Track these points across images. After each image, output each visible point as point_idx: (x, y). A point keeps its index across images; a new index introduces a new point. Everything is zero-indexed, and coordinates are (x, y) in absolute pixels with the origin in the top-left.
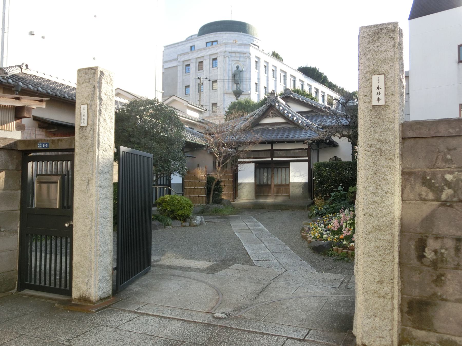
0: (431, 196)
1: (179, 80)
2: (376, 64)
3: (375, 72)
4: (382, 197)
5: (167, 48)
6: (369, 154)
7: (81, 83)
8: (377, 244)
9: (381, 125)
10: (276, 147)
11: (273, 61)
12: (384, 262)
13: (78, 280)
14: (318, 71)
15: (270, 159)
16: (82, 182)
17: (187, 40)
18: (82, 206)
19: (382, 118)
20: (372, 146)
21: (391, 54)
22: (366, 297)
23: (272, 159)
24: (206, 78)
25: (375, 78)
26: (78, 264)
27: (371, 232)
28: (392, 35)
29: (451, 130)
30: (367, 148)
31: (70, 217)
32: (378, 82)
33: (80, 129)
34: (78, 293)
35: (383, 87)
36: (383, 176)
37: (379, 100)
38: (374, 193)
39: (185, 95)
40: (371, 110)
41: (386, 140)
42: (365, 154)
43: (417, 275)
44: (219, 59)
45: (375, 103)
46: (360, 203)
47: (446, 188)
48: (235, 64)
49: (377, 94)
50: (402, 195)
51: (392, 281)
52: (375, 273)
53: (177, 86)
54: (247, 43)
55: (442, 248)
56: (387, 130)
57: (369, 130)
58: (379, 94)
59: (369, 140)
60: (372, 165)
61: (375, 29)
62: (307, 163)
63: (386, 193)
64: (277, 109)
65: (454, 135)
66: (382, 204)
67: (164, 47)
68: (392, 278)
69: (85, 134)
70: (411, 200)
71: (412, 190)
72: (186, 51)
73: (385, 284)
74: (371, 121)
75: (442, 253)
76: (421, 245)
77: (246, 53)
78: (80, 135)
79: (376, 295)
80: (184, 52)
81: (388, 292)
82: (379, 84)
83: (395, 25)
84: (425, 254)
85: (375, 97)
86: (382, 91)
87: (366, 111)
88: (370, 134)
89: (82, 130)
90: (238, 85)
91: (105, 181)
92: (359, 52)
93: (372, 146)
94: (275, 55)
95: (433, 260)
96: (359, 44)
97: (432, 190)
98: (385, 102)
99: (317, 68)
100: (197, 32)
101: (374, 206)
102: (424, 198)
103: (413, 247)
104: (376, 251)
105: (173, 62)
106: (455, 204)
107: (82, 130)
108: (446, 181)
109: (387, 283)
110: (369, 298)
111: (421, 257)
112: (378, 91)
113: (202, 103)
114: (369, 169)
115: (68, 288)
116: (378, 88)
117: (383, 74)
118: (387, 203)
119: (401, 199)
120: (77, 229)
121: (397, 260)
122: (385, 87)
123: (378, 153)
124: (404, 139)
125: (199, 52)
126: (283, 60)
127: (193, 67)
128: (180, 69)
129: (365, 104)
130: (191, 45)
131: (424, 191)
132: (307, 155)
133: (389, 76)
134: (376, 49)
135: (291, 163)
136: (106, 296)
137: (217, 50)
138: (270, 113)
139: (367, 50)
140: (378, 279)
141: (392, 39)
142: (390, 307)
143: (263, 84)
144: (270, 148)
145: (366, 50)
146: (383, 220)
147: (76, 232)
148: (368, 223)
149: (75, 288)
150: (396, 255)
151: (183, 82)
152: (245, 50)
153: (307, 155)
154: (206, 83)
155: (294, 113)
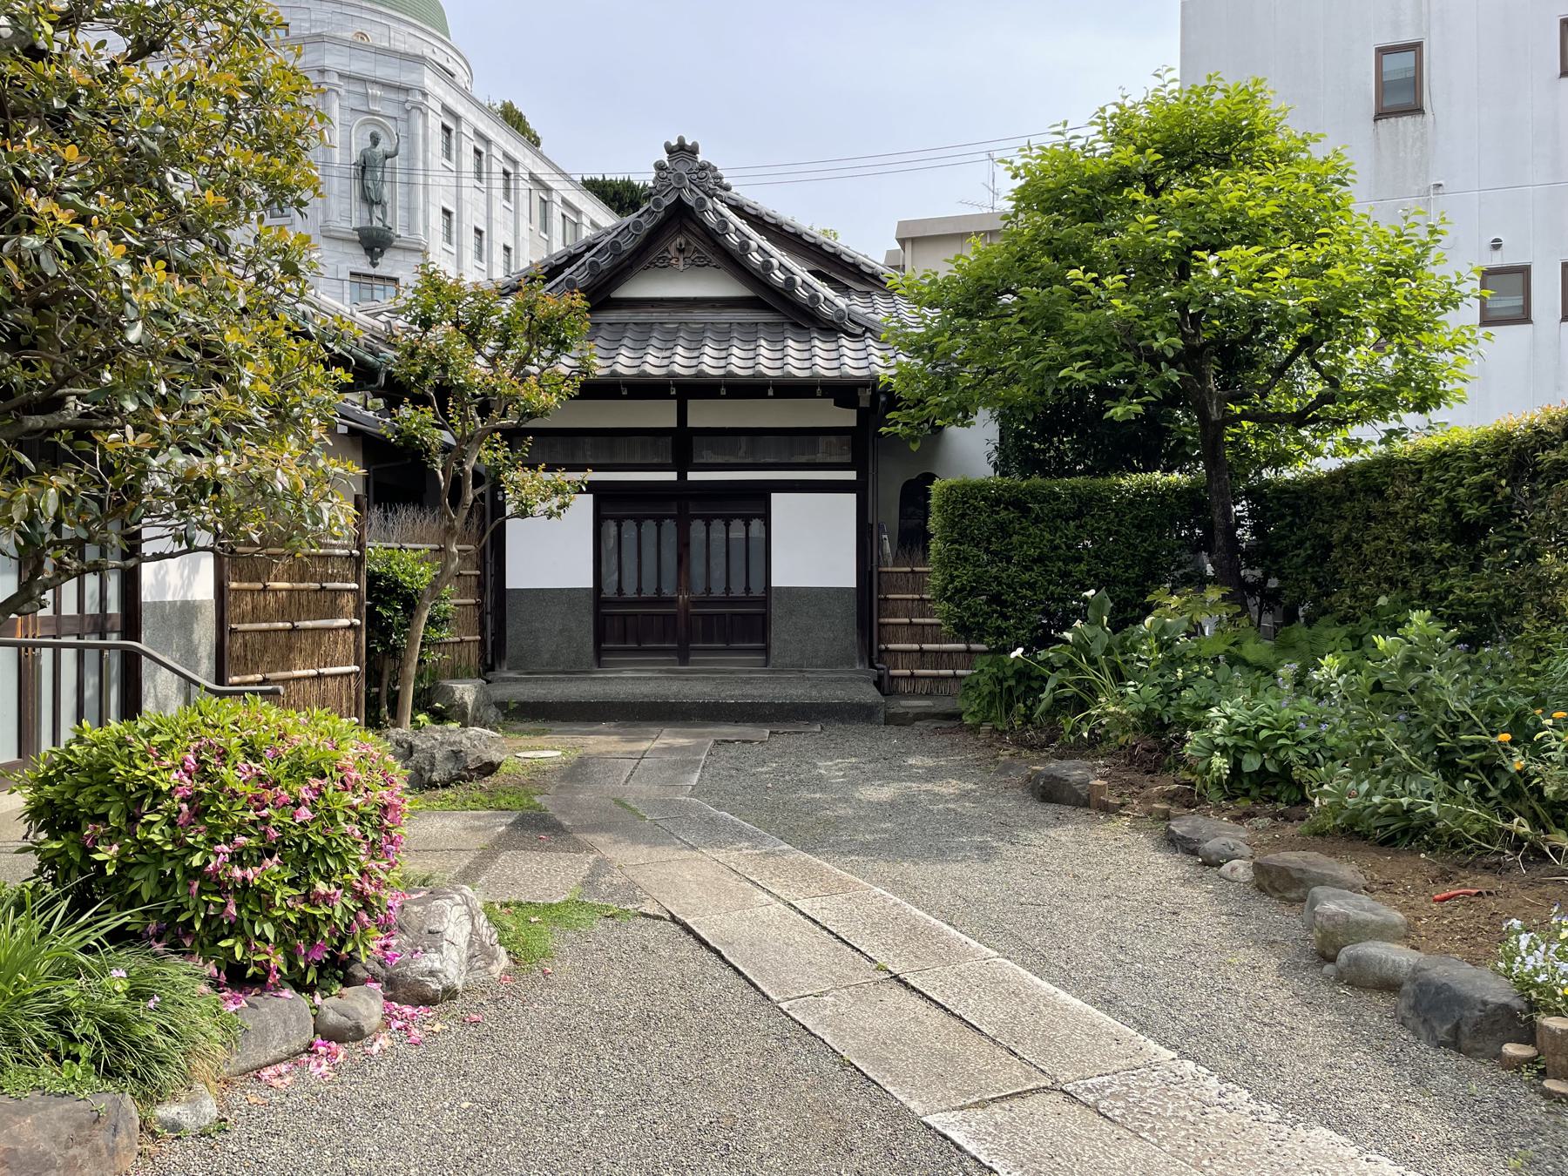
10: (703, 415)
11: (503, 139)
15: (672, 476)
23: (682, 476)
48: (364, 123)
62: (850, 499)
77: (407, 90)
90: (377, 211)
94: (512, 119)
126: (538, 145)
132: (847, 458)
135: (776, 498)
138: (672, 249)
142: (1089, 1072)
144: (671, 422)
152: (406, 78)
153: (847, 458)
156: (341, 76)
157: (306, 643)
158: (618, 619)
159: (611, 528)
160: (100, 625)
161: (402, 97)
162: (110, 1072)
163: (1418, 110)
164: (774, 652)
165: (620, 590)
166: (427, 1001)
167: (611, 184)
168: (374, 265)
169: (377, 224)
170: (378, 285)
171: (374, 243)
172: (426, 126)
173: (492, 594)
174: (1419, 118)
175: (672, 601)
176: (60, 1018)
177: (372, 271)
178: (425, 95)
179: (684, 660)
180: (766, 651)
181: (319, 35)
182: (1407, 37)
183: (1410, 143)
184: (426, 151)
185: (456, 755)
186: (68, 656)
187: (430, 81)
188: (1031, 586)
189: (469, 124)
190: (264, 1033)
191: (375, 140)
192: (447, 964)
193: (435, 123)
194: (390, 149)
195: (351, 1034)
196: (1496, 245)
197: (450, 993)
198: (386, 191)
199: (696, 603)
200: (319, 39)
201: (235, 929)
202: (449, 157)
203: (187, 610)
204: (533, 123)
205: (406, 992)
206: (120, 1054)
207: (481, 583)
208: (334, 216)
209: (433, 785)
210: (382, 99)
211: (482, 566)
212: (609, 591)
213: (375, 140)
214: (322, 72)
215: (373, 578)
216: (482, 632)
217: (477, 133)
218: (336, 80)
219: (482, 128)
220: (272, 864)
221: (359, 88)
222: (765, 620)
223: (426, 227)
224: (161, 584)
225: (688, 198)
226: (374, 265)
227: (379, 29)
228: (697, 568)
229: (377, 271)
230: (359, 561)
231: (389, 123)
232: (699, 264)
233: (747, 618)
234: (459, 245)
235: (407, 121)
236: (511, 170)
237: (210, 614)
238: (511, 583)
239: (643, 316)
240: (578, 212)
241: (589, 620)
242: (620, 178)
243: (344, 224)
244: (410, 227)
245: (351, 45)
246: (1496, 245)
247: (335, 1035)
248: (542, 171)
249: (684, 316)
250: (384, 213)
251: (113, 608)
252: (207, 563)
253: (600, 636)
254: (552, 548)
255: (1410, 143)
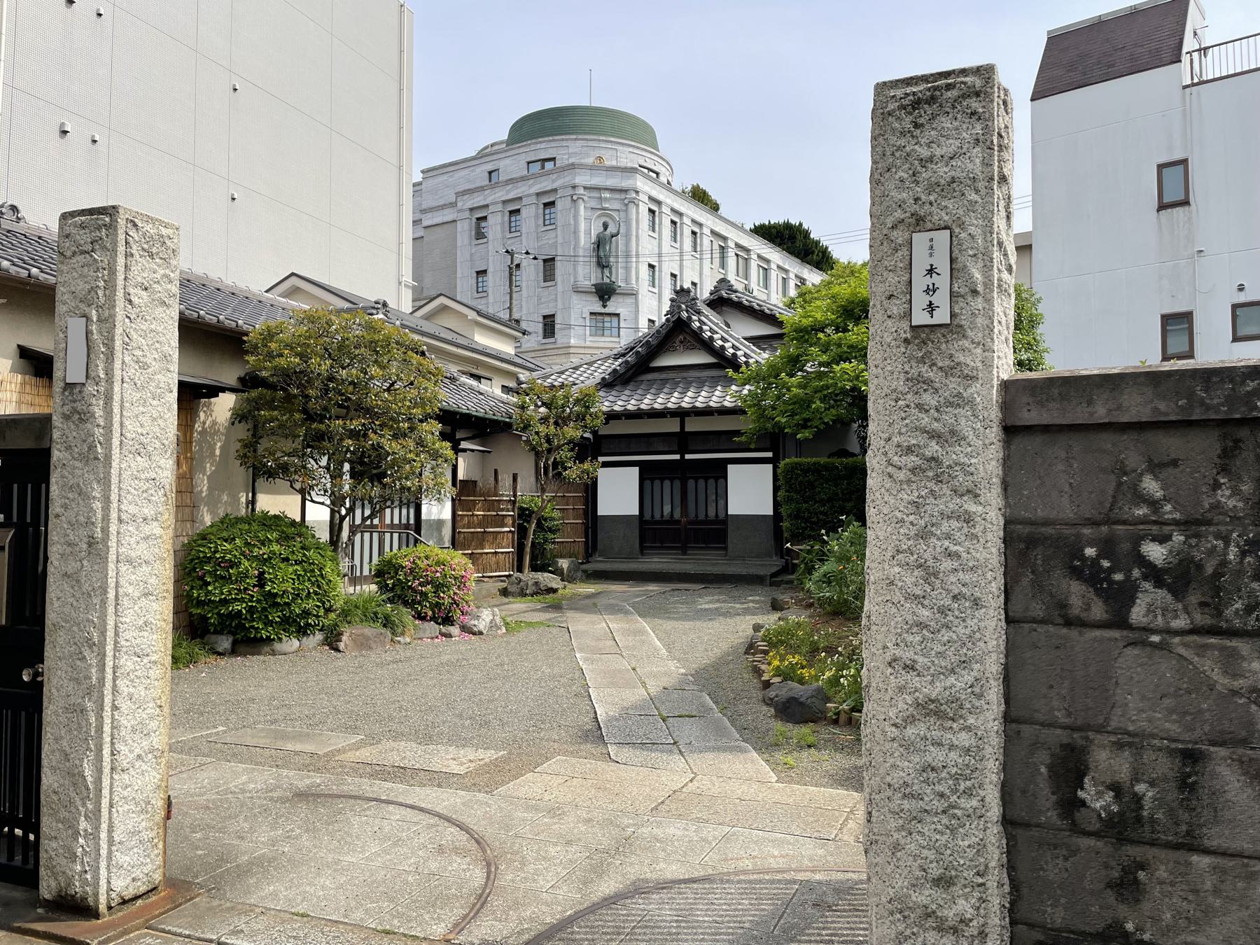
0: (1098, 611)
1: (463, 255)
2: (923, 197)
3: (919, 223)
4: (943, 611)
5: (430, 174)
6: (902, 475)
7: (68, 254)
8: (929, 759)
9: (937, 385)
10: (693, 426)
11: (692, 211)
12: (954, 816)
13: (54, 845)
14: (806, 234)
15: (677, 457)
16: (69, 550)
17: (482, 155)
18: (67, 621)
19: (940, 364)
20: (909, 450)
21: (970, 166)
22: (901, 927)
23: (683, 457)
24: (527, 253)
25: (920, 239)
26: (55, 798)
27: (910, 720)
28: (975, 104)
29: (1162, 406)
30: (896, 458)
31: (34, 651)
32: (931, 255)
33: (65, 389)
34: (53, 884)
35: (944, 267)
36: (946, 543)
37: (931, 308)
38: (916, 597)
39: (476, 295)
40: (906, 341)
41: (953, 432)
42: (890, 476)
43: (1060, 861)
44: (559, 205)
45: (920, 318)
46: (874, 628)
47: (1147, 585)
48: (599, 216)
49: (927, 291)
50: (1006, 604)
51: (980, 880)
52: (925, 852)
53: (455, 272)
54: (629, 165)
55: (1136, 779)
56: (958, 401)
57: (900, 403)
58: (930, 290)
59: (900, 434)
60: (912, 509)
61: (921, 88)
63: (955, 597)
64: (694, 332)
65: (1173, 418)
66: (943, 631)
67: (423, 172)
68: (982, 868)
69: (78, 406)
70: (1034, 621)
71: (1038, 586)
72: (478, 184)
73: (957, 890)
74: (906, 373)
75: (1135, 794)
76: (1070, 769)
77: (626, 191)
78: (66, 408)
79: (931, 922)
80: (472, 186)
81: (968, 916)
82: (931, 261)
83: (986, 72)
84: (1080, 794)
85: (920, 300)
86: (943, 281)
87: (893, 343)
88: (903, 415)
89: (72, 394)
90: (607, 272)
91: (143, 545)
92: (874, 162)
93: (909, 450)
94: (699, 196)
95: (1111, 815)
96: (874, 138)
97: (1099, 592)
98: (953, 315)
99: (794, 221)
100: (504, 136)
101: (918, 638)
102: (1078, 618)
103: (1043, 769)
104: (926, 781)
105: (446, 211)
106: (1177, 640)
107: (72, 394)
108: (1143, 562)
109: (965, 886)
110: (908, 932)
111: (1071, 805)
112: (928, 281)
113: (516, 316)
114: (902, 521)
115: (31, 866)
116: (931, 271)
117: (946, 228)
118: (961, 630)
119: (1003, 617)
120: (54, 690)
121: (995, 812)
122: (952, 269)
123: (931, 474)
124: (1011, 431)
125: (509, 187)
127: (495, 225)
128: (464, 229)
129: (889, 322)
130: (490, 167)
131: (1077, 594)
133: (963, 235)
134: (924, 152)
135: (731, 468)
136: (143, 889)
137: (554, 181)
139: (897, 154)
140: (935, 871)
141: (974, 118)
143: (669, 266)
145: (893, 154)
146: (948, 684)
147: (50, 700)
148: (901, 689)
149: (47, 868)
150: (992, 795)
151: (471, 260)
152: (625, 184)
154: (526, 262)
155: (737, 340)
156: (585, 188)
157: (490, 538)
158: (651, 531)
159: (647, 483)
160: (407, 526)
161: (623, 196)
162: (385, 626)
163: (1186, 203)
164: (730, 549)
165: (652, 516)
166: (474, 634)
167: (776, 226)
168: (604, 306)
169: (607, 280)
170: (607, 319)
171: (605, 292)
172: (638, 213)
173: (591, 519)
174: (1187, 208)
175: (678, 522)
176: (375, 614)
177: (603, 311)
178: (637, 192)
179: (685, 554)
180: (725, 549)
181: (573, 164)
182: (1178, 156)
183: (1181, 224)
184: (637, 229)
185: (536, 583)
186: (396, 536)
187: (641, 183)
188: (825, 514)
189: (667, 205)
190: (425, 631)
191: (605, 226)
192: (482, 625)
193: (644, 209)
194: (615, 231)
195: (449, 636)
196: (1241, 288)
197: (481, 633)
198: (612, 259)
199: (691, 523)
200: (572, 166)
201: (419, 603)
202: (654, 231)
203: (440, 523)
204: (714, 195)
205: (465, 629)
206: (387, 623)
207: (586, 512)
208: (581, 278)
209: (526, 595)
210: (611, 199)
211: (586, 504)
212: (647, 516)
213: (605, 226)
214: (574, 187)
215: (521, 509)
216: (586, 537)
217: (673, 210)
218: (581, 191)
219: (677, 206)
220: (429, 587)
221: (595, 194)
222: (725, 531)
223: (637, 279)
224: (429, 512)
225: (684, 315)
226: (604, 306)
227: (611, 152)
228: (692, 506)
229: (607, 310)
230: (514, 502)
231: (615, 214)
232: (691, 348)
233: (715, 531)
234: (660, 287)
235: (626, 211)
236: (697, 230)
237: (449, 524)
238: (601, 511)
239: (664, 376)
240: (747, 251)
241: (637, 532)
242: (781, 221)
243: (587, 283)
244: (627, 280)
245: (592, 168)
246: (1241, 288)
247: (443, 635)
248: (721, 228)
249: (685, 374)
250: (611, 273)
251: (412, 522)
252: (448, 505)
253: (642, 539)
254: (619, 492)
255: (1181, 224)
